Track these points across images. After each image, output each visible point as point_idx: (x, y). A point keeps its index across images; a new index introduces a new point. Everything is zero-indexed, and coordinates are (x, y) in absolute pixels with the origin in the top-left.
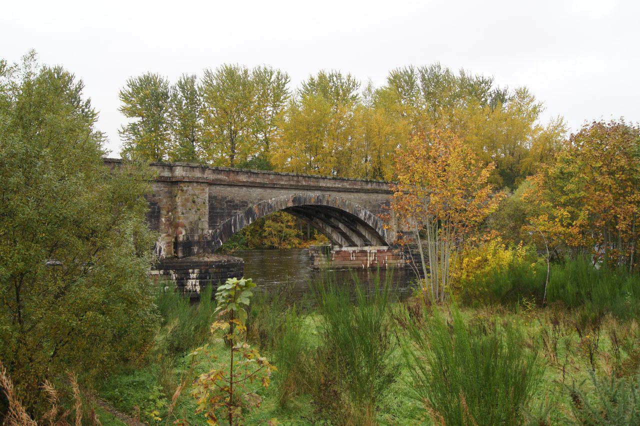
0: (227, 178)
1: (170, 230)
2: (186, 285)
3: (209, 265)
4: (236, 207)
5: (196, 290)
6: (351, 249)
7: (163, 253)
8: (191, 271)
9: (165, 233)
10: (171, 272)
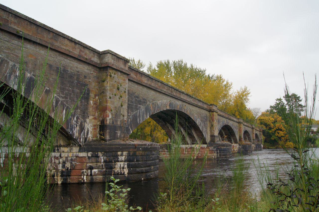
0: (135, 77)
1: (97, 113)
2: (115, 168)
3: (135, 146)
4: (140, 102)
5: (124, 173)
6: (184, 146)
7: (90, 135)
8: (119, 153)
9: (93, 116)
10: (100, 154)
